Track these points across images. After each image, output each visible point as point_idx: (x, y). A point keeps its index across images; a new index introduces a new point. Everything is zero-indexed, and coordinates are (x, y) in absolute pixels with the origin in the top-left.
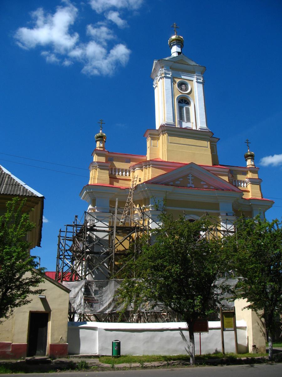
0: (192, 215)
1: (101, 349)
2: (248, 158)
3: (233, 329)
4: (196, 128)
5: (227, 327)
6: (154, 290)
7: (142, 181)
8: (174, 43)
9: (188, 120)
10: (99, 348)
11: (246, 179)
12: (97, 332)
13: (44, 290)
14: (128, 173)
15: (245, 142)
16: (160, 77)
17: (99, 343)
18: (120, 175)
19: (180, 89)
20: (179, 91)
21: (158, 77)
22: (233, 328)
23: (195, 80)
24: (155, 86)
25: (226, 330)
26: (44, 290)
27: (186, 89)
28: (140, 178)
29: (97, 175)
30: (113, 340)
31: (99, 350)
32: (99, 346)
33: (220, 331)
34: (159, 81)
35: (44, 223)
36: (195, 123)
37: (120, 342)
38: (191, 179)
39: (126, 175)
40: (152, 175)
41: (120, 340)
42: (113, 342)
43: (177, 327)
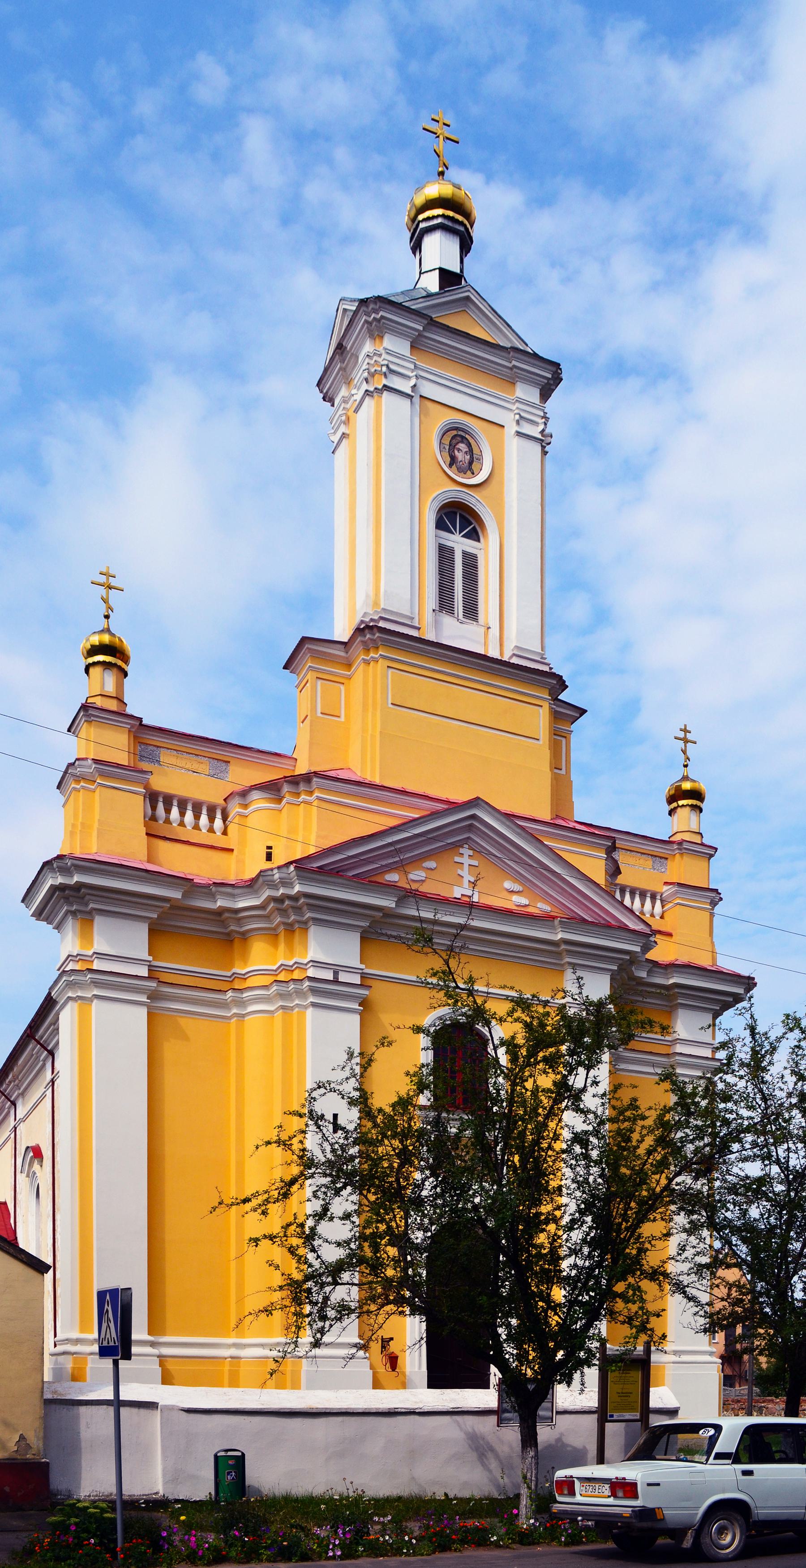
0: (590, 920)
1: (173, 1477)
2: (681, 803)
3: (637, 1415)
4: (501, 654)
5: (617, 1409)
6: (320, 1296)
7: (279, 859)
8: (434, 217)
9: (471, 611)
10: (164, 1475)
11: (666, 888)
12: (158, 1413)
13: (41, 1166)
14: (218, 823)
15: (676, 738)
16: (365, 387)
17: (165, 1457)
18: (189, 828)
19: (448, 459)
20: (440, 465)
21: (354, 391)
22: (638, 1414)
23: (508, 419)
24: (339, 434)
25: (615, 1418)
26: (41, 1166)
27: (469, 468)
28: (270, 848)
29: (97, 817)
30: (218, 1446)
31: (165, 1483)
32: (164, 1470)
33: (593, 1419)
34: (356, 411)
35: (71, 834)
36: (495, 631)
37: (243, 1455)
38: (466, 867)
39: (211, 830)
40: (318, 837)
41: (240, 1445)
42: (216, 1457)
43: (449, 1405)
